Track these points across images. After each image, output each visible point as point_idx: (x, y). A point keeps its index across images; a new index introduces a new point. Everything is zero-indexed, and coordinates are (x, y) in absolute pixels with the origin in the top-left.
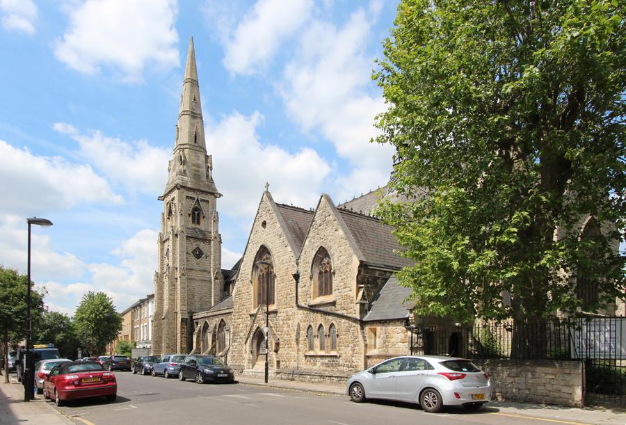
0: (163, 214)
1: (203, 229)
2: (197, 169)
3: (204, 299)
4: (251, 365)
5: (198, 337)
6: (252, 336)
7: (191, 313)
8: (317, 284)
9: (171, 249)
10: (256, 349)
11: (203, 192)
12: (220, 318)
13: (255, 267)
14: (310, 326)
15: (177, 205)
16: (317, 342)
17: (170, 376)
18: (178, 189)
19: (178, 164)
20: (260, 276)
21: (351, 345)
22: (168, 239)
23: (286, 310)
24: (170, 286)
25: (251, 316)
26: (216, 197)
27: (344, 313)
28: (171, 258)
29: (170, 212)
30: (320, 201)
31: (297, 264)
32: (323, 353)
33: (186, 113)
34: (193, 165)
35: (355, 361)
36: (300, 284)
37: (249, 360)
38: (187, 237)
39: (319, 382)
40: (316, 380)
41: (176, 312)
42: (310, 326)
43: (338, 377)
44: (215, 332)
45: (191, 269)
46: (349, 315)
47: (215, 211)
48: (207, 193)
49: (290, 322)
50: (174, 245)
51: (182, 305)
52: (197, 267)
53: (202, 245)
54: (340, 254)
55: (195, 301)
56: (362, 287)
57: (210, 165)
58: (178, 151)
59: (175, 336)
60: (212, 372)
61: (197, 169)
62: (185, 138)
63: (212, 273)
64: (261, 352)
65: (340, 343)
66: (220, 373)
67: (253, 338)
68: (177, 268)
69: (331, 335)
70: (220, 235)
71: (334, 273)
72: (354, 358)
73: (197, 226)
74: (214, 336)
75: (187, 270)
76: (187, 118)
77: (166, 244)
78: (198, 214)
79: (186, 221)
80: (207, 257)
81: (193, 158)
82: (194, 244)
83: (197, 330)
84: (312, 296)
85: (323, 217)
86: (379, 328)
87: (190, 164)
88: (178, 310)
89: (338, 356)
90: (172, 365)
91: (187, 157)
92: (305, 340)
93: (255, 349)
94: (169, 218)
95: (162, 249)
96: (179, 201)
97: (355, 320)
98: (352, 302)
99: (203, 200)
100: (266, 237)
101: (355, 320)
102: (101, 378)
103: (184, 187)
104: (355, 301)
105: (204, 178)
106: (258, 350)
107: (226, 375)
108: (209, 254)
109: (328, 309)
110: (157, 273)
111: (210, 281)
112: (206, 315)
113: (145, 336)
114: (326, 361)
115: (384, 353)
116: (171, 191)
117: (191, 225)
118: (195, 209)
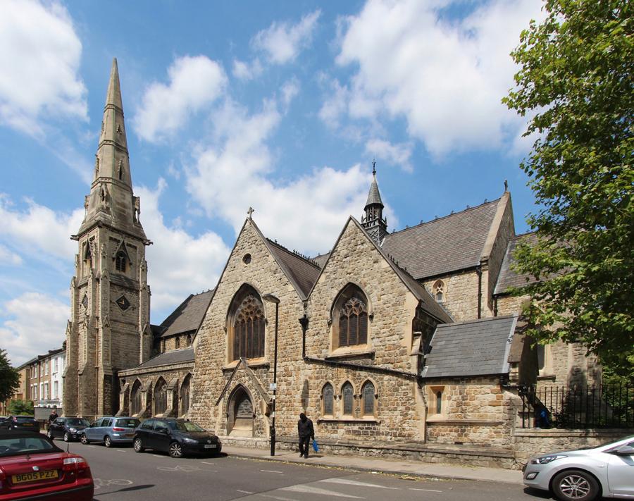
0: (78, 256)
1: (130, 277)
2: (123, 208)
3: (131, 355)
4: (225, 430)
5: (126, 397)
6: (227, 395)
7: (116, 370)
8: (338, 331)
9: (89, 295)
10: (233, 412)
11: (129, 235)
12: (159, 376)
13: (232, 309)
14: (328, 384)
15: (98, 245)
16: (339, 404)
17: (115, 445)
18: (100, 227)
19: (99, 198)
20: (237, 322)
21: (402, 408)
22: (86, 284)
23: (285, 363)
24: (89, 337)
25: (224, 371)
26: (145, 244)
27: (390, 367)
28: (90, 306)
29: (88, 255)
30: (346, 226)
31: (305, 306)
32: (349, 418)
33: (108, 143)
34: (118, 203)
35: (407, 428)
36: (310, 331)
37: (223, 424)
38: (111, 283)
39: (347, 454)
40: (341, 452)
41: (97, 368)
42: (328, 384)
43: (382, 449)
44: (150, 391)
45: (115, 321)
46: (397, 370)
47: (144, 259)
48: (134, 237)
49: (290, 379)
50: (94, 290)
51: (105, 360)
52: (122, 319)
53: (128, 295)
54: (383, 292)
55: (120, 357)
56: (419, 335)
57: (137, 208)
58: (99, 184)
59: (96, 394)
60: (195, 441)
61: (123, 208)
62: (107, 170)
63: (140, 327)
64: (239, 415)
65: (380, 405)
66: (208, 444)
67: (230, 398)
68: (98, 318)
69: (364, 395)
70: (149, 286)
71: (371, 317)
72: (405, 425)
73: (123, 274)
74: (149, 396)
75: (111, 323)
76: (109, 149)
77: (82, 292)
78: (124, 260)
79: (110, 265)
80: (134, 309)
81: (119, 196)
82: (120, 292)
83: (124, 389)
84: (330, 346)
85: (352, 245)
86: (448, 388)
87: (114, 202)
88: (100, 365)
89: (378, 421)
90: (117, 430)
91: (110, 192)
92: (318, 401)
93: (232, 412)
94: (85, 261)
95: (77, 296)
96: (101, 241)
97: (409, 377)
98: (403, 353)
99: (130, 245)
100: (251, 274)
101: (409, 377)
102: (60, 471)
103: (108, 227)
104: (409, 352)
105: (131, 221)
106: (236, 413)
107: (214, 446)
108: (136, 306)
109: (360, 362)
110: (70, 323)
111: (138, 336)
112: (137, 372)
113: (46, 394)
114: (356, 428)
115: (459, 419)
116: (89, 230)
117: (115, 271)
118: (120, 254)
